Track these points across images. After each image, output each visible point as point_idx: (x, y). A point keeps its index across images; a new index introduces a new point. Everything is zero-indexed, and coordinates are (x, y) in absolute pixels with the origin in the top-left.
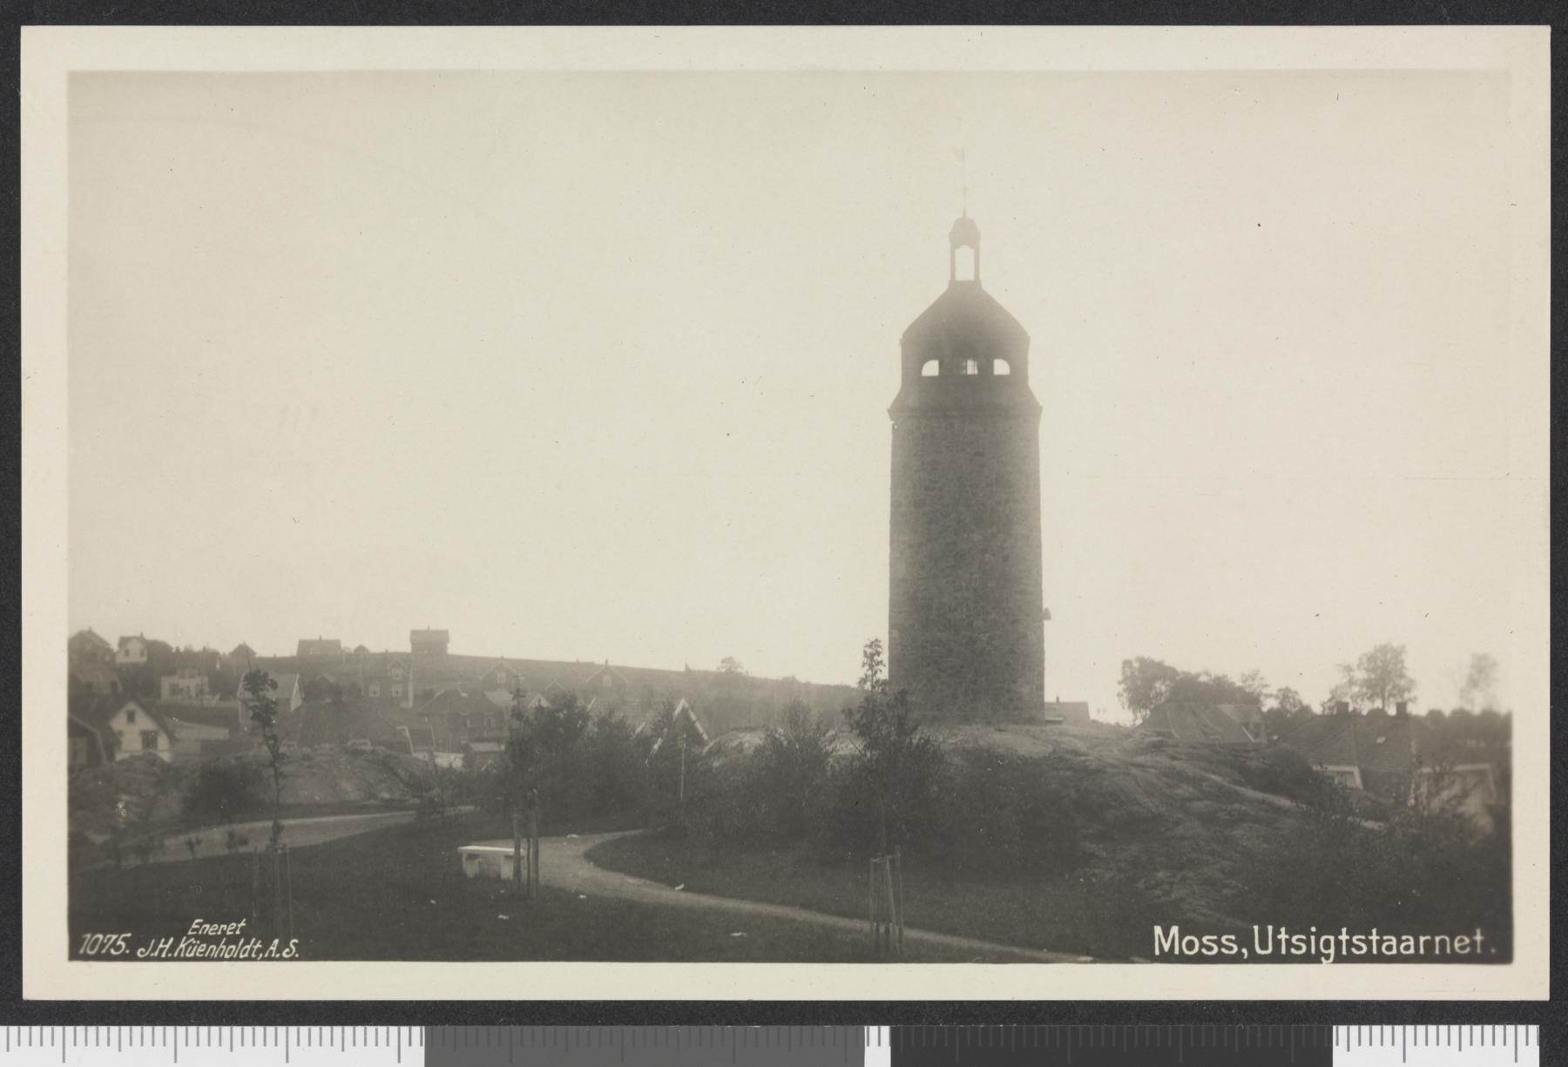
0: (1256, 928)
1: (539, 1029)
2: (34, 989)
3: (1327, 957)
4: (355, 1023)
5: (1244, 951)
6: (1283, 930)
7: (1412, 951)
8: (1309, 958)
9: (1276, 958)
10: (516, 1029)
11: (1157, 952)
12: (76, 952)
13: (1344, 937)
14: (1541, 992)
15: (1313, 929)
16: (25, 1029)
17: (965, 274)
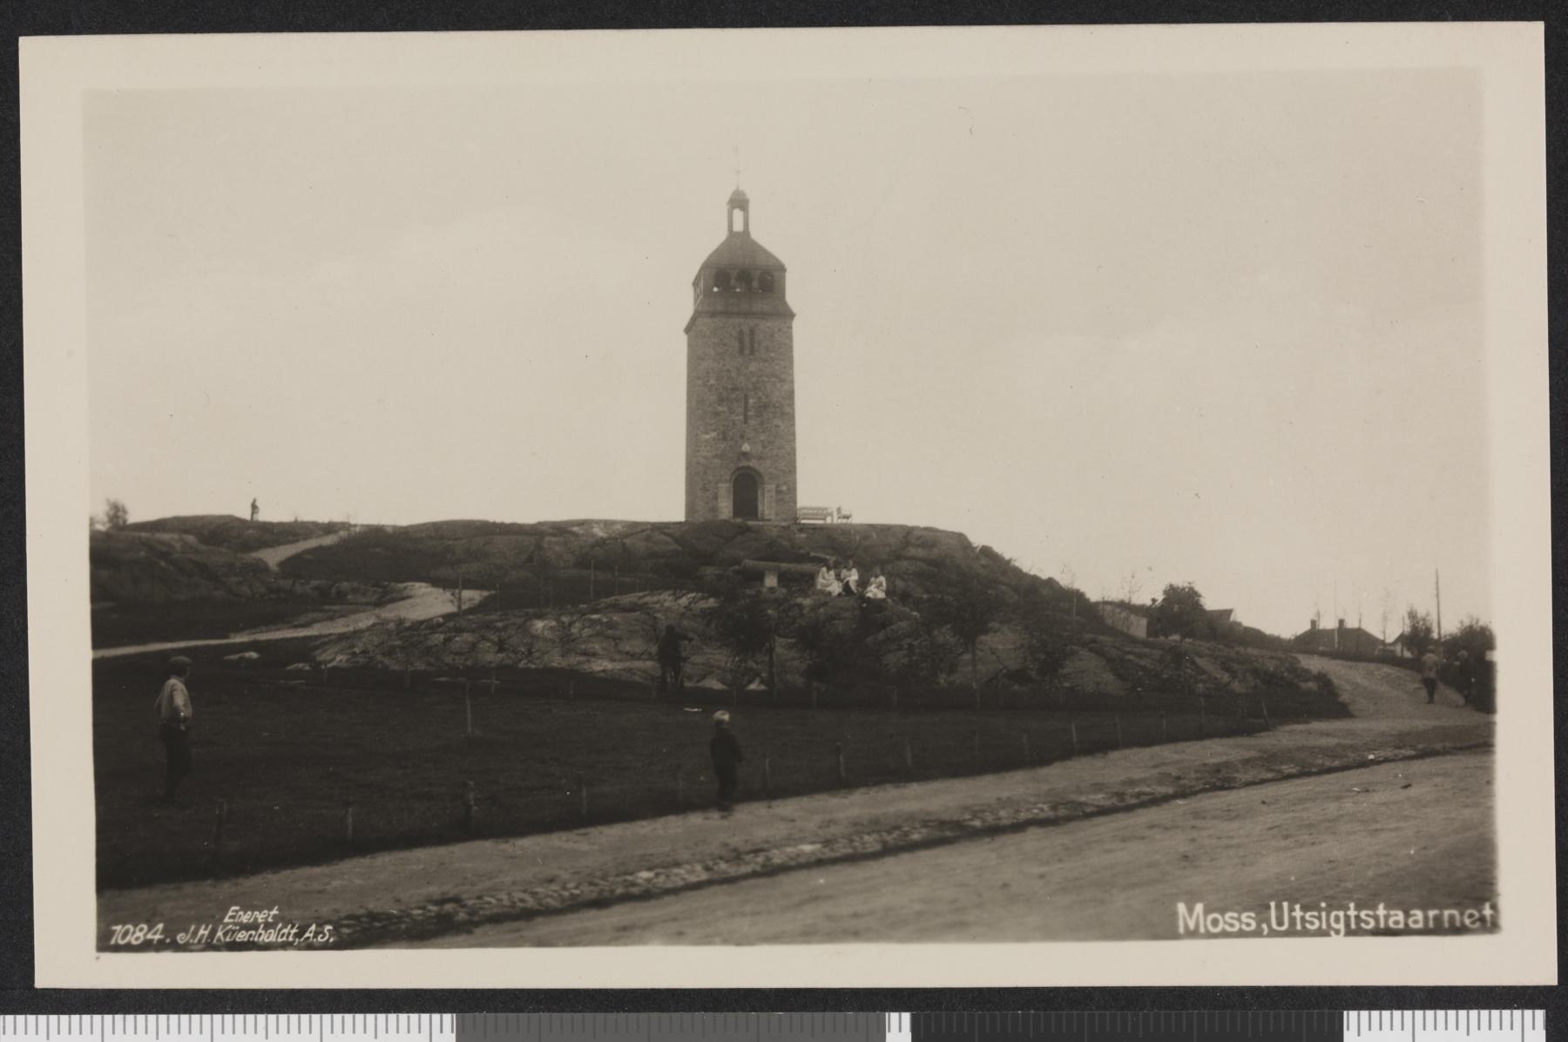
2: (47, 976)
3: (1337, 932)
4: (81, 1011)
8: (1321, 933)
9: (1291, 933)
10: (545, 1016)
11: (1181, 930)
12: (105, 944)
13: (1352, 913)
14: (1547, 974)
15: (1323, 905)
16: (64, 1018)
17: (738, 227)
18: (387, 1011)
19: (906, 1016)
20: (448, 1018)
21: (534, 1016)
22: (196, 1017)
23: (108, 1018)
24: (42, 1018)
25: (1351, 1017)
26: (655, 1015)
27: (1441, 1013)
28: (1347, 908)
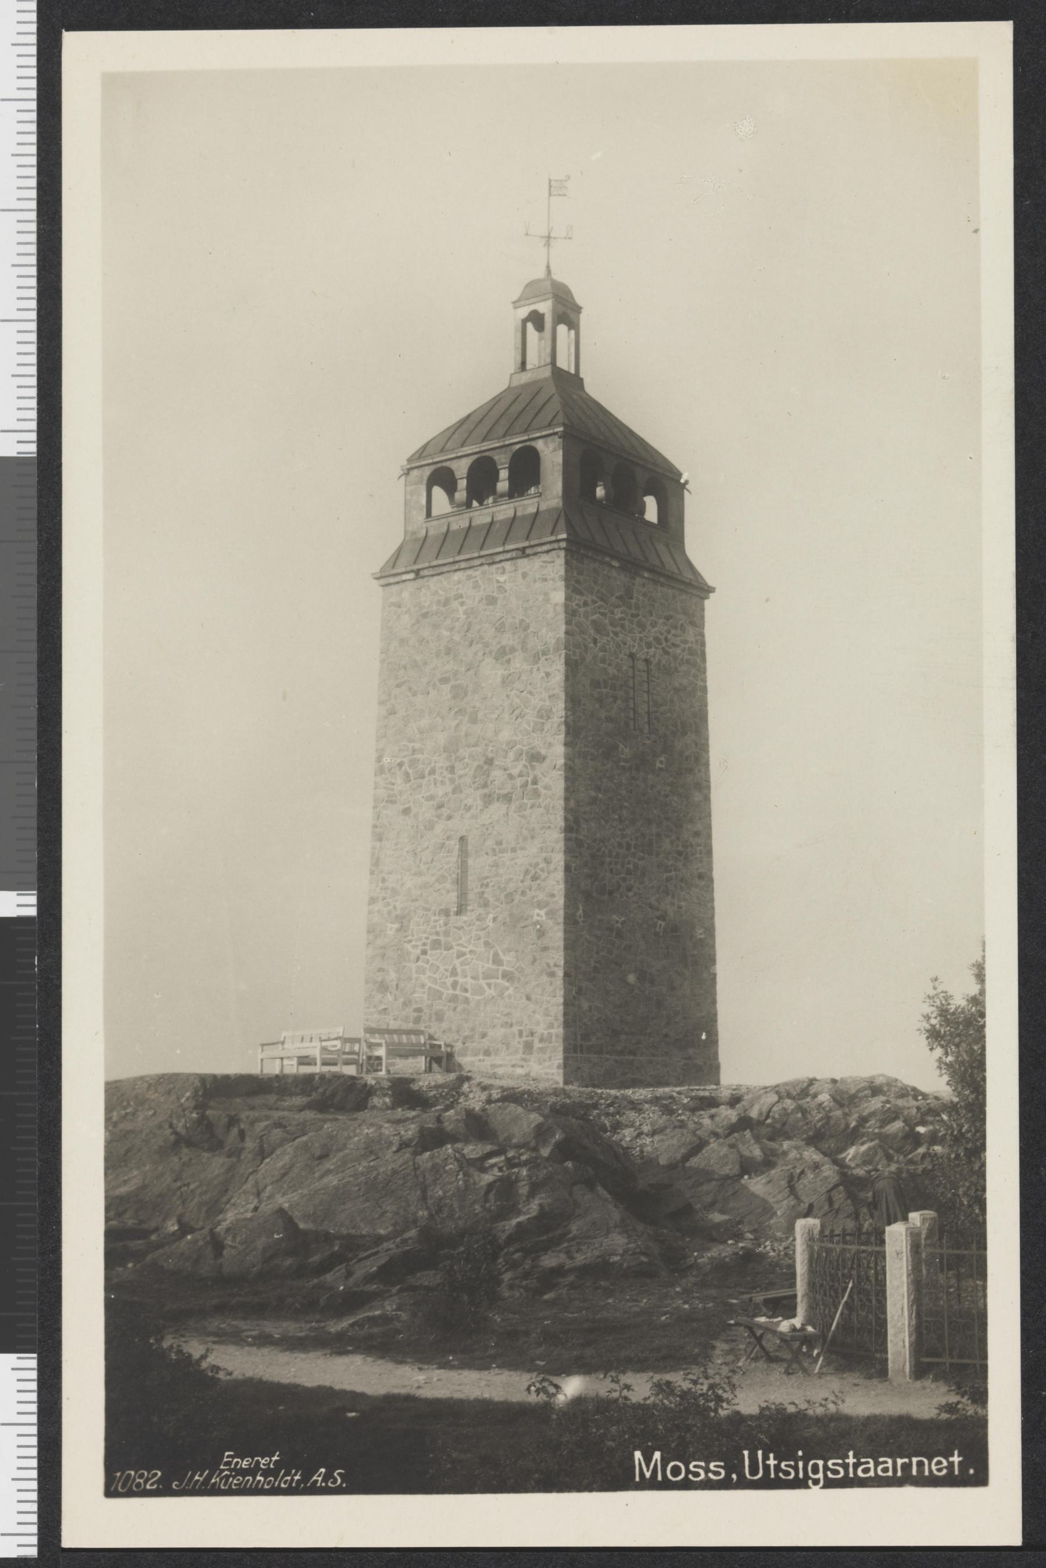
0: (746, 1453)
1: (34, 569)
3: (816, 1482)
5: (734, 1476)
6: (772, 1456)
7: (890, 1474)
8: (799, 1484)
13: (851, 1460)
19: (32, 912)
22: (33, 194)
23: (34, 105)
26: (34, 657)
27: (34, 1452)
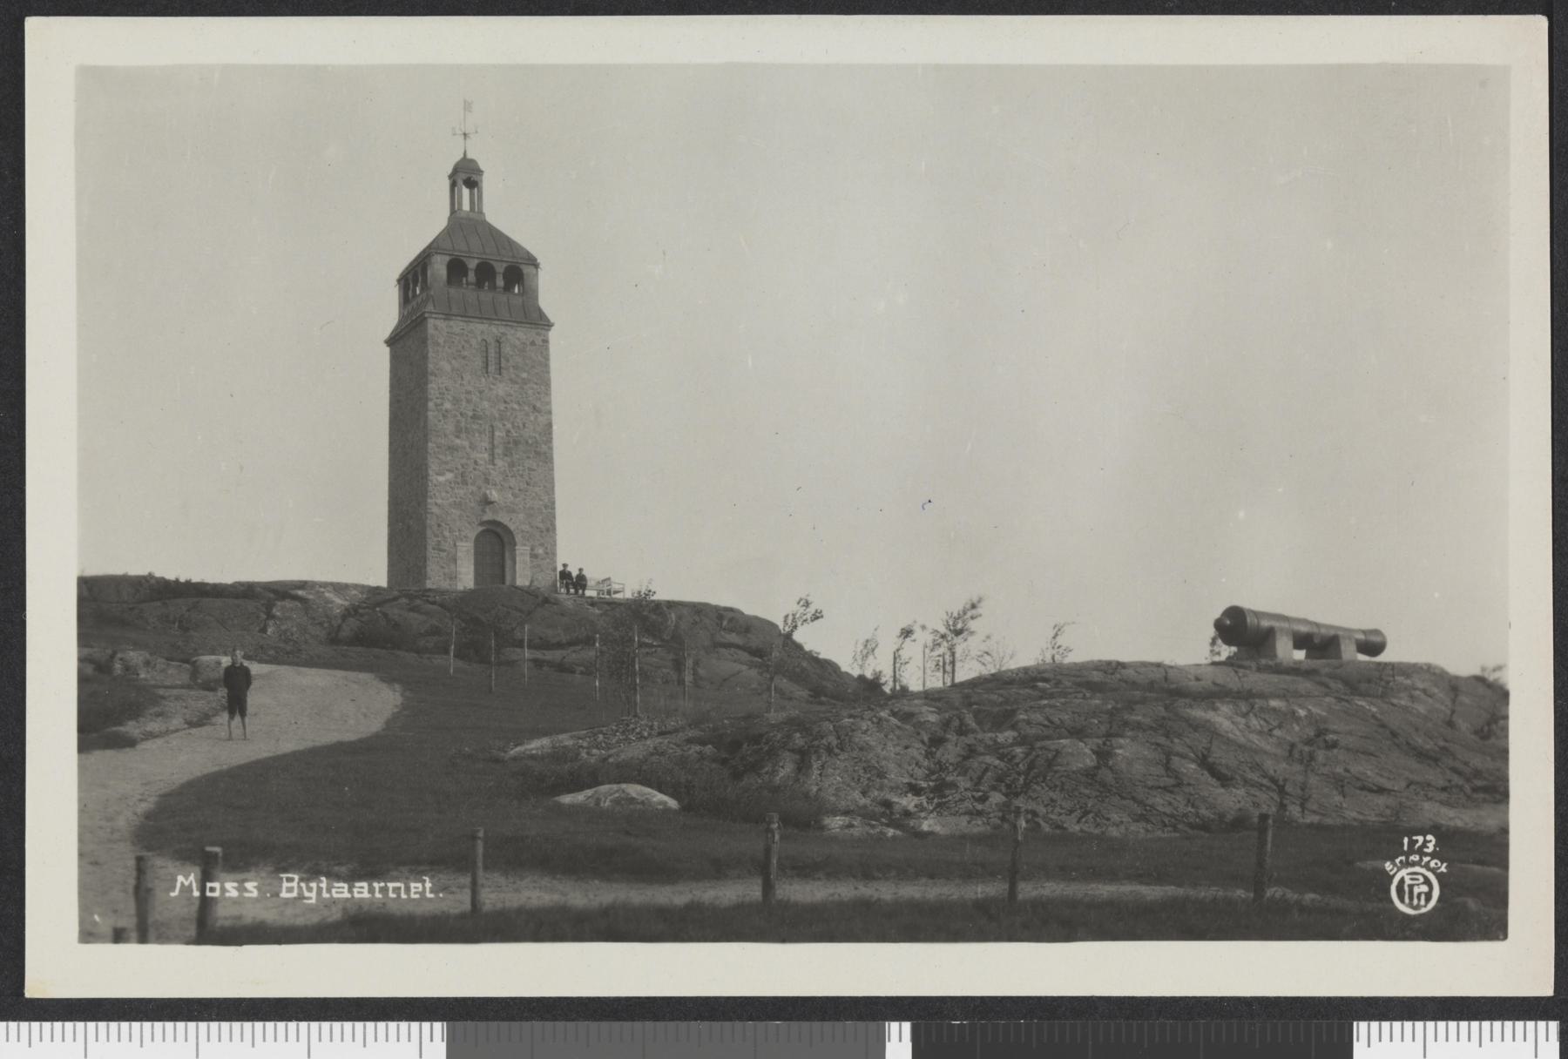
18: (230, 1019)
19: (907, 1026)
20: (438, 1026)
21: (526, 1025)
23: (91, 1025)
24: (24, 1025)
25: (1361, 1028)
28: (424, 882)
